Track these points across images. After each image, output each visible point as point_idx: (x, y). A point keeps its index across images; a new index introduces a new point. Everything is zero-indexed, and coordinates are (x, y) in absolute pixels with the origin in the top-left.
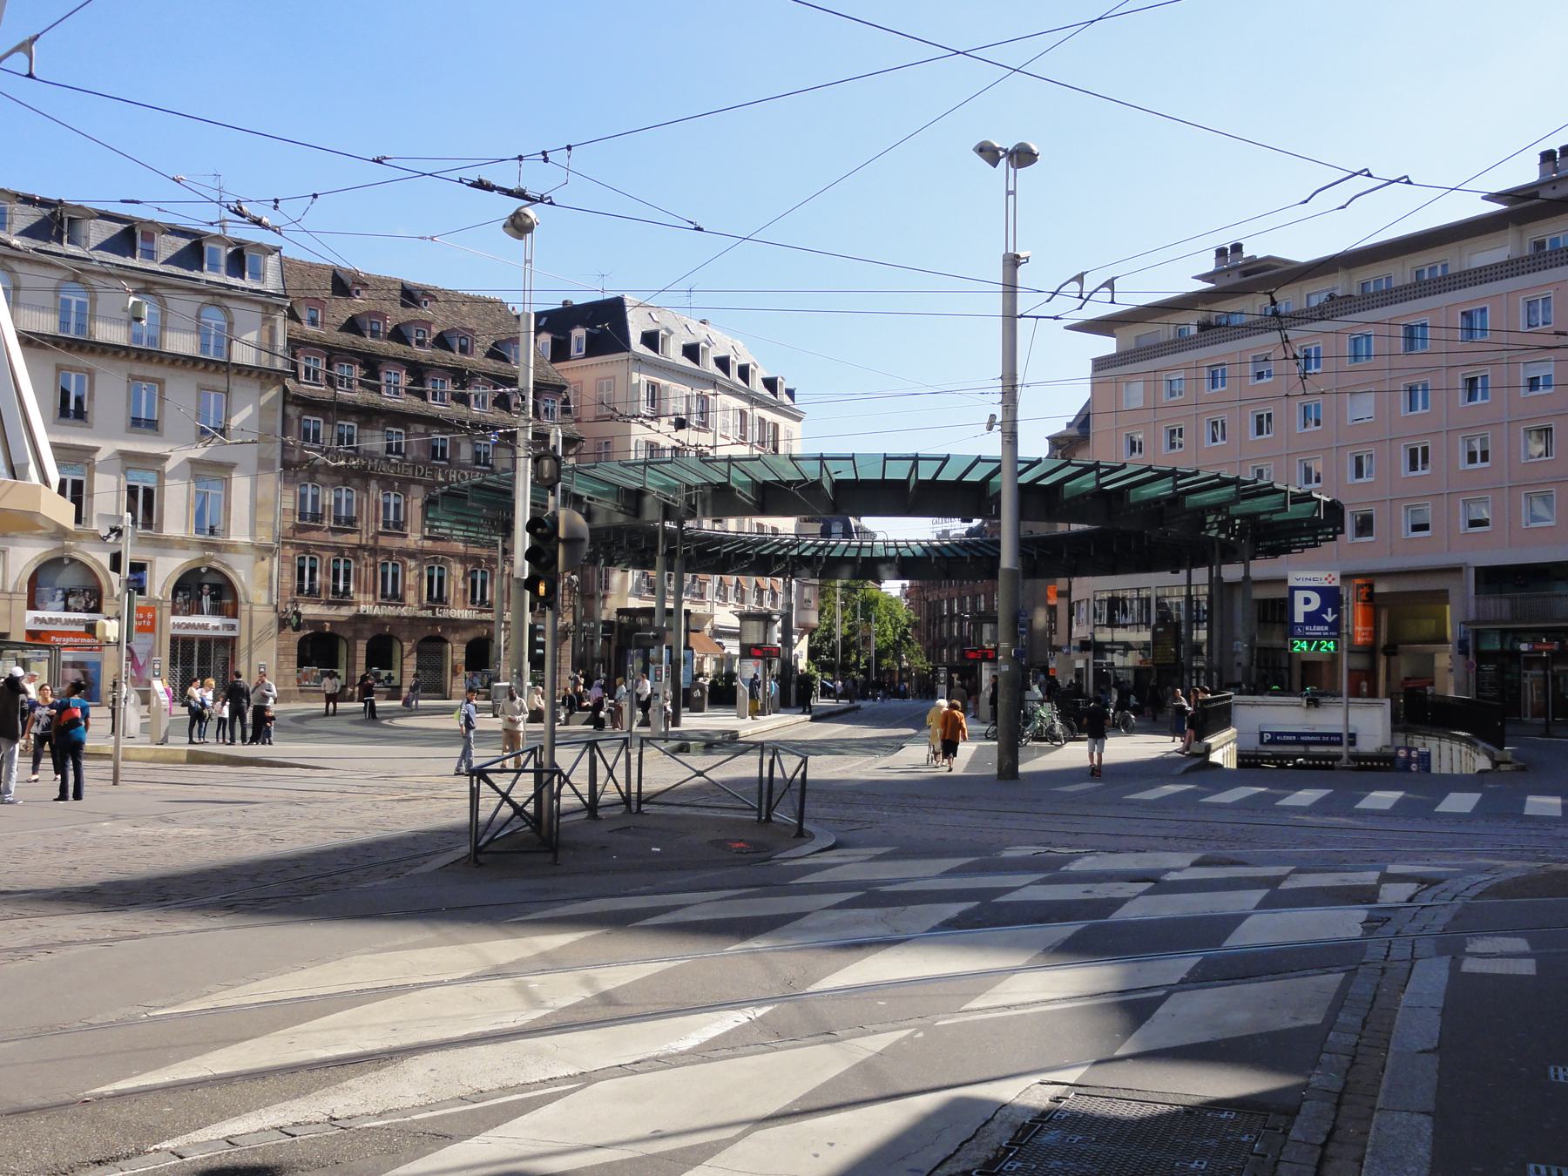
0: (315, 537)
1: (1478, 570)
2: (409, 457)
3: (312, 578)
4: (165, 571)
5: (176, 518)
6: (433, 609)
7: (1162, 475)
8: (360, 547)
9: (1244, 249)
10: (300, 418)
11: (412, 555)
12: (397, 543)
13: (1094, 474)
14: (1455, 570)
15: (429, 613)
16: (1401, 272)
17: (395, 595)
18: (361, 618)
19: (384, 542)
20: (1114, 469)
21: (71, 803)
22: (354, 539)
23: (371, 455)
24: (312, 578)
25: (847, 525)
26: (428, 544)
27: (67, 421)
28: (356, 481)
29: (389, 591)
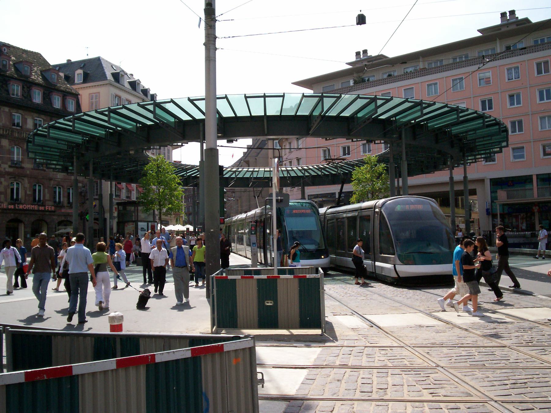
1: (491, 180)
6: (14, 204)
7: (453, 110)
9: (368, 52)
13: (419, 108)
14: (482, 181)
15: (12, 207)
16: (447, 59)
20: (429, 105)
21: (487, 98)
25: (60, 258)
29: (15, 197)
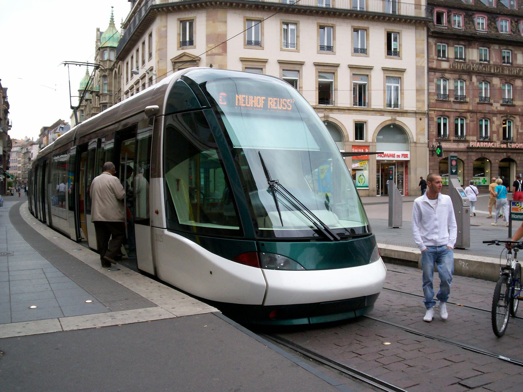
0: (445, 107)
2: (491, 62)
3: (433, 110)
4: (373, 124)
5: (377, 98)
6: (506, 143)
8: (469, 111)
10: (436, 44)
11: (495, 114)
12: (487, 108)
15: (504, 146)
17: (486, 137)
18: (470, 149)
19: (480, 108)
22: (465, 107)
23: (473, 62)
24: (433, 110)
26: (503, 108)
27: (357, 54)
28: (465, 77)
